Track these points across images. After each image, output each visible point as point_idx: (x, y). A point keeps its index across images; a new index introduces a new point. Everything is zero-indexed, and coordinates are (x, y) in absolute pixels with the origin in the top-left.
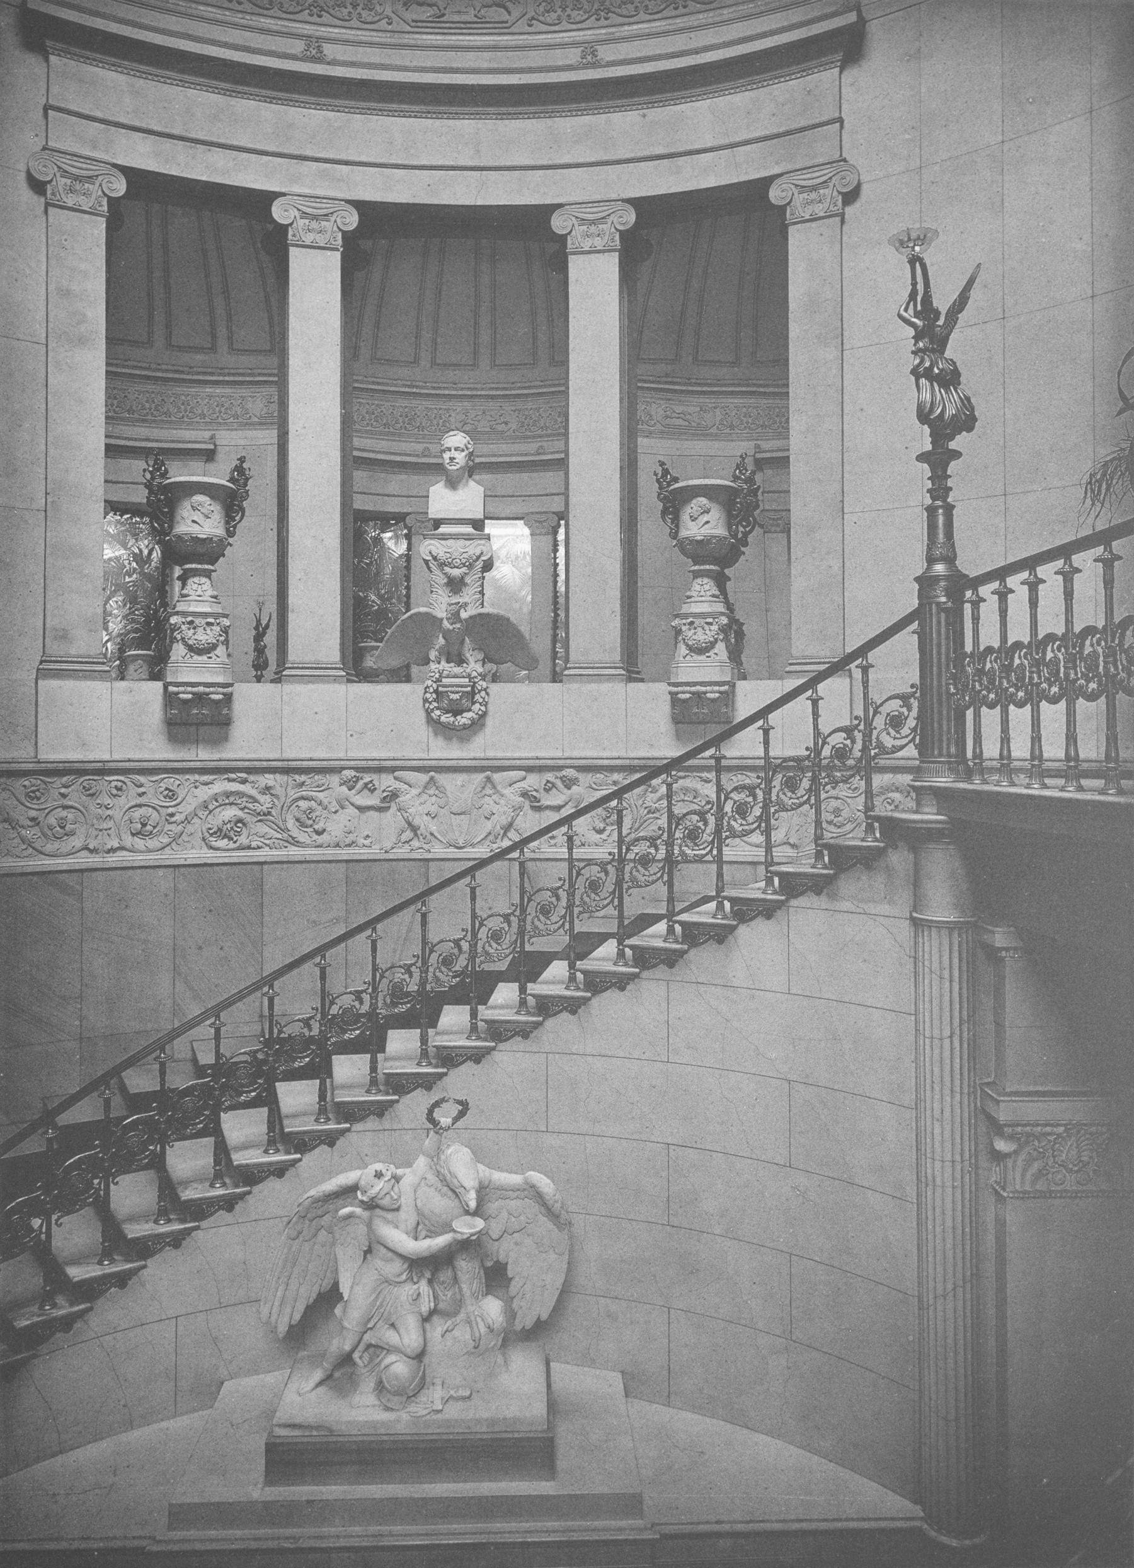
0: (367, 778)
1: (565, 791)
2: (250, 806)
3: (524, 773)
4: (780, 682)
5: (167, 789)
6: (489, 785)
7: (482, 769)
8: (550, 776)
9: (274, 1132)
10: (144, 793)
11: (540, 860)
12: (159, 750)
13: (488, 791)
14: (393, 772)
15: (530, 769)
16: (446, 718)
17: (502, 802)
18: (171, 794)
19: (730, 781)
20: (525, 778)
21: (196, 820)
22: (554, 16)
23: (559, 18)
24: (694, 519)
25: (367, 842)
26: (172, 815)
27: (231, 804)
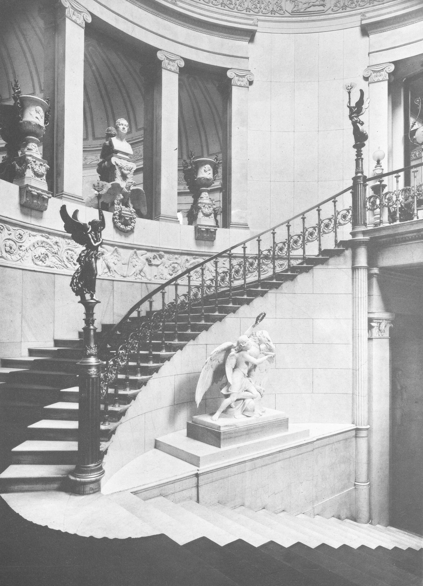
1: (160, 260)
2: (50, 249)
3: (146, 252)
5: (20, 234)
6: (135, 255)
7: (132, 248)
8: (155, 254)
9: (201, 309)
10: (11, 234)
12: (16, 215)
13: (135, 257)
15: (148, 250)
16: (122, 227)
17: (139, 261)
18: (21, 237)
20: (146, 254)
21: (29, 251)
22: (354, 5)
23: (356, 5)
24: (205, 171)
26: (21, 246)
27: (43, 247)
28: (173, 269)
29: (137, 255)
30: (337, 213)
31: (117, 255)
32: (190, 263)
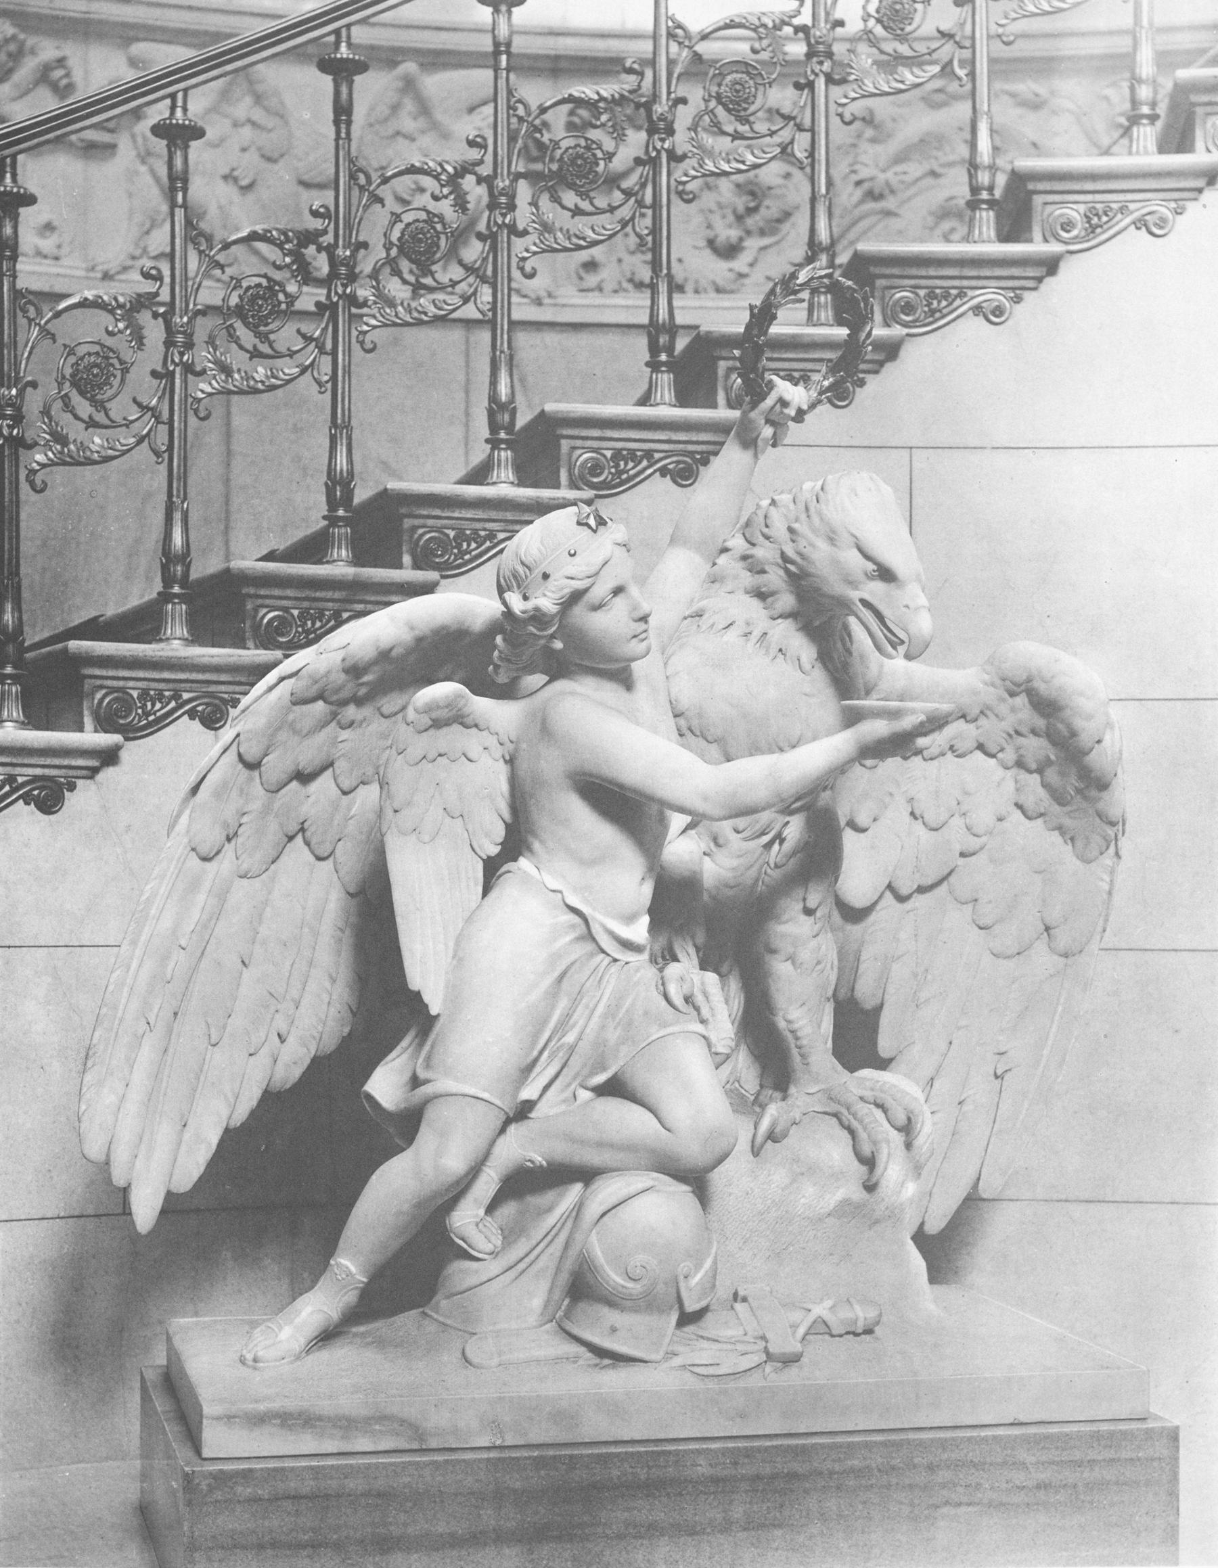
0: (48, 50)
4: (205, 1421)
11: (552, 325)
13: (408, 124)
14: (128, 41)
19: (630, 182)
25: (47, 244)
28: (741, 203)
29: (424, 109)
30: (357, 179)
31: (258, 115)
32: (892, 147)
